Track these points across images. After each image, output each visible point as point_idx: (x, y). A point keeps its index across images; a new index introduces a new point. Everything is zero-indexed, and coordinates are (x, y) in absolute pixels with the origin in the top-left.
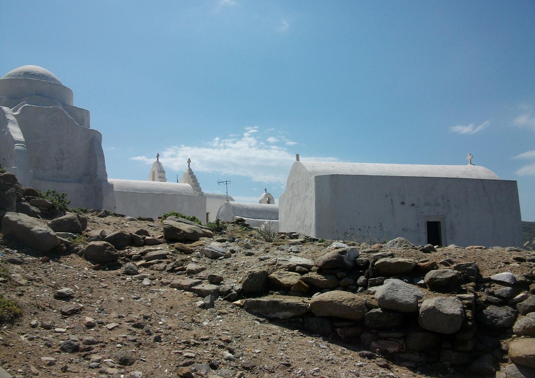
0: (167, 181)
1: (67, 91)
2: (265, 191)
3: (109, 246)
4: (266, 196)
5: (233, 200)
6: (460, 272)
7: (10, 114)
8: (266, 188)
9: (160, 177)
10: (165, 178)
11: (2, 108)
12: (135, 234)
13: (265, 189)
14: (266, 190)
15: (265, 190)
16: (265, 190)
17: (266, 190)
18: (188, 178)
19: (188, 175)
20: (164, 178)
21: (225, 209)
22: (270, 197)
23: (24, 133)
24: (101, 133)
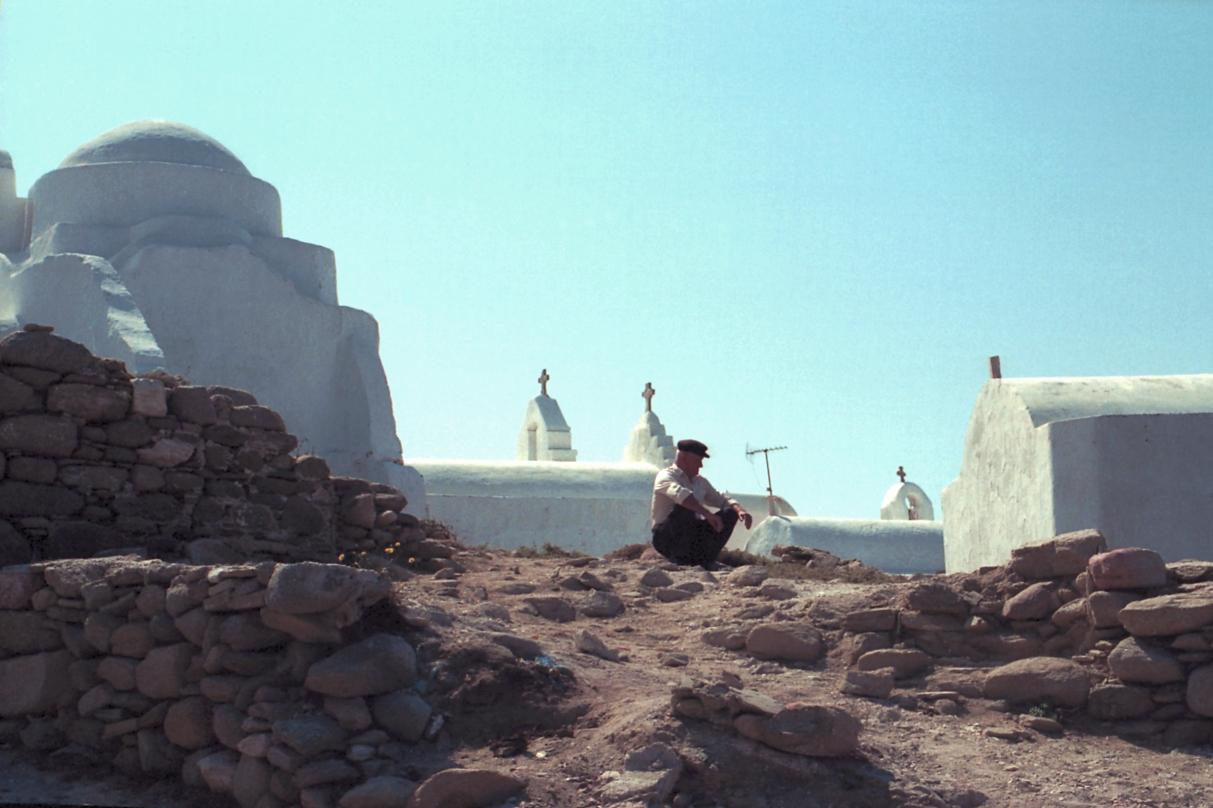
0: (577, 457)
1: (265, 195)
2: (899, 478)
3: (930, 691)
4: (902, 493)
5: (795, 514)
6: (478, 761)
7: (109, 276)
8: (901, 468)
9: (553, 448)
10: (570, 449)
11: (82, 259)
12: (107, 560)
13: (898, 470)
14: (901, 473)
15: (899, 473)
16: (899, 473)
17: (901, 473)
18: (647, 444)
19: (649, 434)
20: (568, 448)
21: (767, 543)
22: (917, 496)
23: (155, 330)
24: (916, 483)
